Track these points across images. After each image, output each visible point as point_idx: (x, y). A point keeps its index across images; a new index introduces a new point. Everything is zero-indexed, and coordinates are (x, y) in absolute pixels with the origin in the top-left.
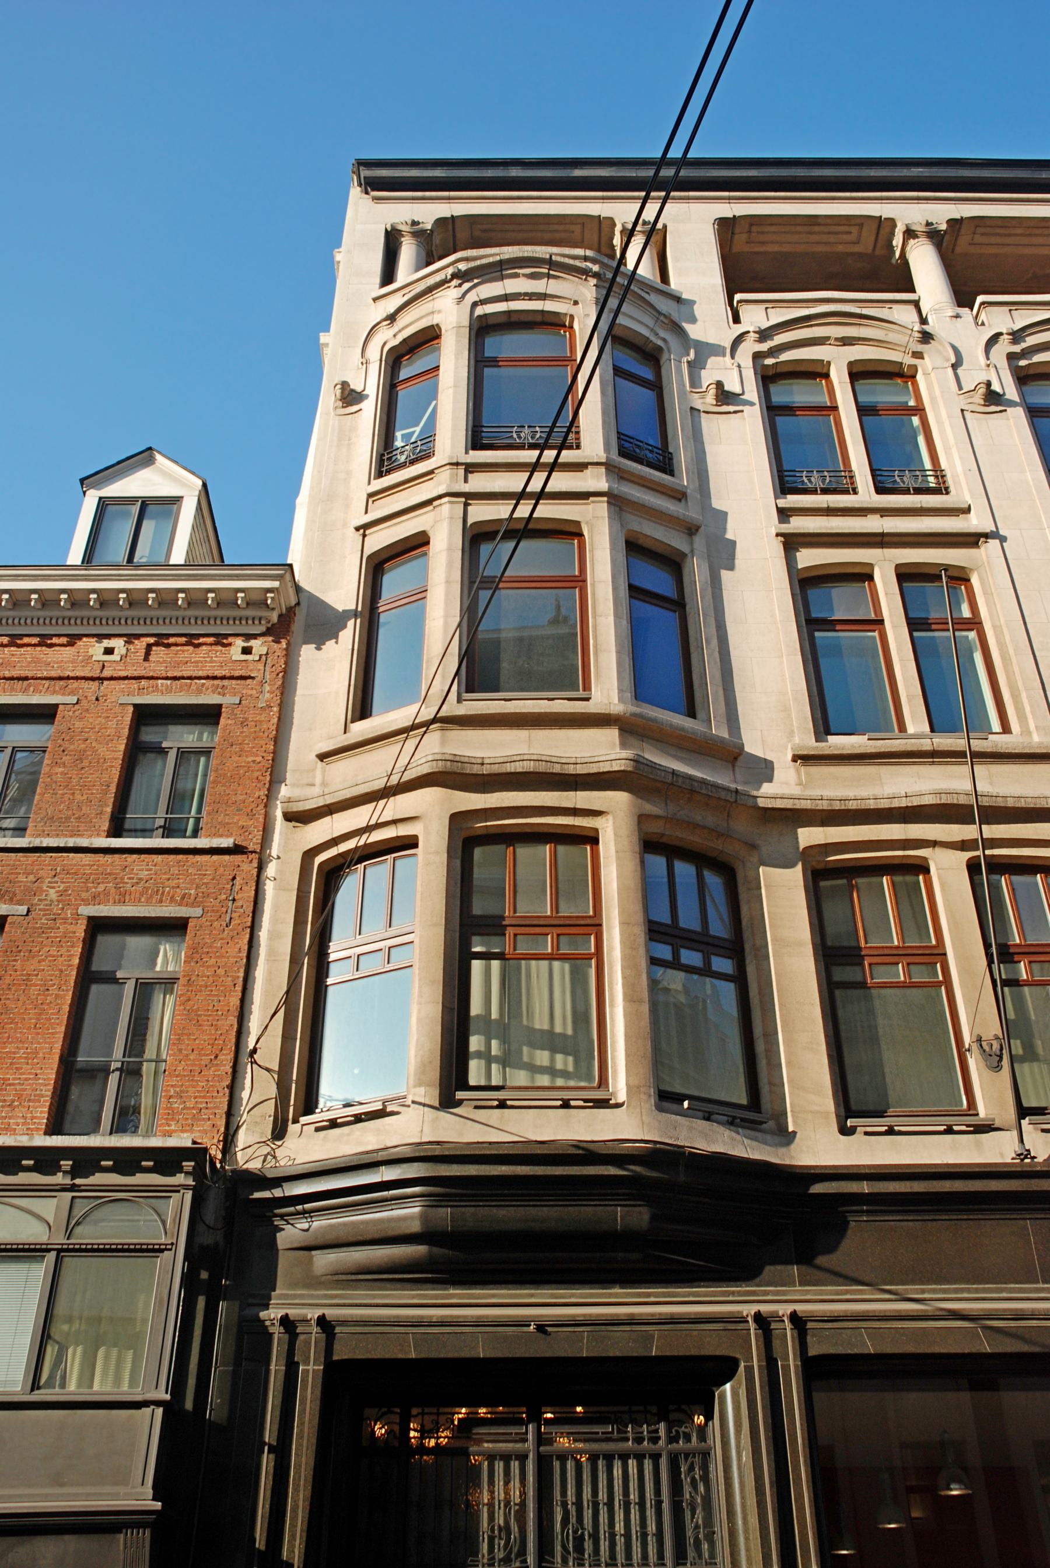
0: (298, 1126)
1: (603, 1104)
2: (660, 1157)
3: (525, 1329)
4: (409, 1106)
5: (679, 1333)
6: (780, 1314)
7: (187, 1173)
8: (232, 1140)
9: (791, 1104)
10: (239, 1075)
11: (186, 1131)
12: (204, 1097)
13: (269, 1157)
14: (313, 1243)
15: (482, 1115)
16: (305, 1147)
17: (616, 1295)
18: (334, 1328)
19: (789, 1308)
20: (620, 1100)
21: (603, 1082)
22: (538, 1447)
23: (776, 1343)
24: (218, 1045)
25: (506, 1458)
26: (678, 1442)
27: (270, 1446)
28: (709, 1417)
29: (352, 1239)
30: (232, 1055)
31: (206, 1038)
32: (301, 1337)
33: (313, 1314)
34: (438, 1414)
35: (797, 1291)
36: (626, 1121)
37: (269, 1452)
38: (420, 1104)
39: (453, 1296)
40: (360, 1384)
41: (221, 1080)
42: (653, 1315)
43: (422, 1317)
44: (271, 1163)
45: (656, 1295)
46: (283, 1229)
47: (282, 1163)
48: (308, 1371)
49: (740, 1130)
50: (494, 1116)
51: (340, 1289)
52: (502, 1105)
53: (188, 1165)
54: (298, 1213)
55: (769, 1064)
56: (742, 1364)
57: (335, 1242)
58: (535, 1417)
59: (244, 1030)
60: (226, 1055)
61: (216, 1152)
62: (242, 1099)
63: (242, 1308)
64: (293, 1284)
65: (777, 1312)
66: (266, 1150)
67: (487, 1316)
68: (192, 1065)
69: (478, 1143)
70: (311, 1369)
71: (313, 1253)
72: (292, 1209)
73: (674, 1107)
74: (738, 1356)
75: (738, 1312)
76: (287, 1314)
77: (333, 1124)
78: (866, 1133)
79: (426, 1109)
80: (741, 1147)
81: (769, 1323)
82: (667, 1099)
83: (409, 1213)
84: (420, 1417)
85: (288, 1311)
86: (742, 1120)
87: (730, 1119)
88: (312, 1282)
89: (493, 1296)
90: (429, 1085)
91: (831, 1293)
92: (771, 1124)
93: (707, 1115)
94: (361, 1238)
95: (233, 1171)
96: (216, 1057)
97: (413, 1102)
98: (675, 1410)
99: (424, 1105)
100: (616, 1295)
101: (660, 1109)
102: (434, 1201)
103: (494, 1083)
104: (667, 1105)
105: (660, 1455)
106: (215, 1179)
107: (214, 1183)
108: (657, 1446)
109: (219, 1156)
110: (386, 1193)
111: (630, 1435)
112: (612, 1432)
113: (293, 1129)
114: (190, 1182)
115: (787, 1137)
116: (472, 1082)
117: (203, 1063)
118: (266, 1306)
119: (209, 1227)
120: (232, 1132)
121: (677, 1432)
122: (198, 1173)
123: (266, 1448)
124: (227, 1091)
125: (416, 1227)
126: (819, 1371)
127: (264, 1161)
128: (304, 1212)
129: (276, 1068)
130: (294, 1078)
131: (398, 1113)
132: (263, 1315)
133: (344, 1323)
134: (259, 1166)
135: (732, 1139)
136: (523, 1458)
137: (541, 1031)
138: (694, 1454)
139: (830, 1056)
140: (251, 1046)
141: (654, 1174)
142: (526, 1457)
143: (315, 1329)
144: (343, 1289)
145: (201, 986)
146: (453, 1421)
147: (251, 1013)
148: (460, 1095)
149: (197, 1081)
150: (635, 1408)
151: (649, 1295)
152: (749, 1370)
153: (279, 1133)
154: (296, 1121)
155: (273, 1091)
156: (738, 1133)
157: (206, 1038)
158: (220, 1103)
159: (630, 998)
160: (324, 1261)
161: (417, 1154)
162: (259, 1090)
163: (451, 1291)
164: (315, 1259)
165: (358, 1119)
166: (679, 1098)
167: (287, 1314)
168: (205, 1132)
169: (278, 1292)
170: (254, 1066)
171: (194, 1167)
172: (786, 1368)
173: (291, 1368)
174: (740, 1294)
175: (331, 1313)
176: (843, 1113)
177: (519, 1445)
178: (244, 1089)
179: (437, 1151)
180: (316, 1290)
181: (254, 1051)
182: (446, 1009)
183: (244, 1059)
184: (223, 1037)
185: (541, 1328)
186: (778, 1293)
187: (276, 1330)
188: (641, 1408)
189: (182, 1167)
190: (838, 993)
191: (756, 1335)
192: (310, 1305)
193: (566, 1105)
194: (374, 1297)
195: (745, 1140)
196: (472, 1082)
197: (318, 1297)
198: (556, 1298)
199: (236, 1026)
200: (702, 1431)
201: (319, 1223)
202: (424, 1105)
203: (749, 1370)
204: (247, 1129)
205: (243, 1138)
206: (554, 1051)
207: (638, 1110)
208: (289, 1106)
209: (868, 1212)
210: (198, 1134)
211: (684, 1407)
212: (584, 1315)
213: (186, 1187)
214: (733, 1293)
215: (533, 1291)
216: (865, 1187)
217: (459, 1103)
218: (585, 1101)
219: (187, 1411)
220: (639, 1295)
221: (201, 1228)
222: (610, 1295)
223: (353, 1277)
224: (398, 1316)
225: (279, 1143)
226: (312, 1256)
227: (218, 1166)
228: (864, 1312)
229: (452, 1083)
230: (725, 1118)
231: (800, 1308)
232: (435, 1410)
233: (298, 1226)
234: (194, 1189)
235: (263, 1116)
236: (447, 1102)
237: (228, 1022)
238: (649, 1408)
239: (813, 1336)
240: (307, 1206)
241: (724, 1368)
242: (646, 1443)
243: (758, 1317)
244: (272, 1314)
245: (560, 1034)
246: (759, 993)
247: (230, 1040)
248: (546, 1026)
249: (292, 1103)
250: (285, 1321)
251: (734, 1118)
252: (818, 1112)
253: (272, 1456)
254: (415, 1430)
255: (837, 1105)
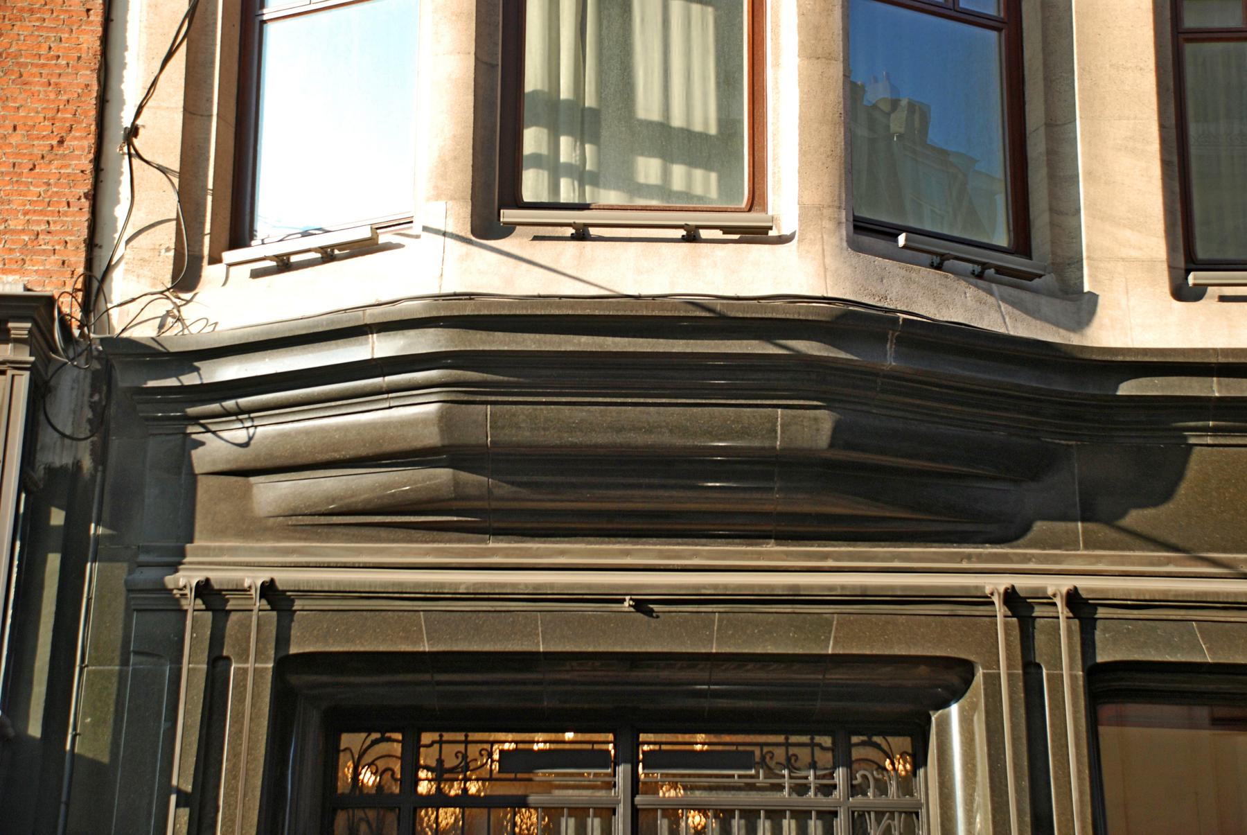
0: (220, 268)
1: (757, 235)
2: (845, 322)
3: (615, 607)
4: (418, 237)
5: (873, 618)
6: (1050, 592)
7: (18, 341)
8: (100, 289)
9: (1088, 246)
10: (108, 177)
11: (11, 272)
12: (41, 213)
13: (170, 320)
14: (253, 465)
15: (545, 252)
16: (231, 302)
17: (769, 555)
18: (291, 601)
19: (1065, 584)
20: (786, 231)
21: (757, 199)
22: (633, 797)
23: (1040, 639)
24: (64, 120)
25: (580, 813)
26: (865, 794)
27: (179, 792)
28: (919, 759)
29: (321, 457)
30: (91, 140)
31: (39, 106)
32: (234, 617)
33: (254, 579)
34: (466, 742)
35: (1080, 558)
36: (799, 265)
37: (178, 805)
38: (437, 232)
39: (494, 552)
40: (330, 694)
41: (73, 183)
42: (831, 588)
43: (442, 585)
44: (174, 330)
45: (838, 557)
46: (202, 444)
47: (194, 329)
48: (245, 671)
49: (994, 286)
50: (567, 254)
51: (300, 539)
52: (581, 235)
53: (20, 328)
54: (227, 413)
55: (1052, 176)
56: (980, 673)
57: (291, 462)
58: (628, 753)
59: (112, 95)
60: (81, 138)
61: (70, 307)
62: (115, 219)
63: (130, 572)
64: (219, 532)
65: (1044, 589)
66: (163, 306)
67: (552, 585)
68: (17, 155)
69: (540, 296)
70: (252, 672)
71: (253, 479)
72: (215, 407)
73: (881, 244)
74: (972, 658)
75: (977, 588)
76: (208, 580)
77: (284, 264)
78: (1223, 299)
79: (450, 242)
80: (997, 316)
81: (1031, 607)
82: (867, 232)
83: (415, 414)
84: (436, 746)
85: (211, 575)
86: (1000, 270)
87: (978, 269)
88: (250, 526)
89: (562, 553)
90: (452, 198)
91: (1141, 561)
92: (1049, 280)
93: (937, 260)
94: (337, 456)
95: (103, 341)
96: (61, 142)
97: (425, 229)
98: (863, 744)
99: (445, 234)
100: (769, 555)
101: (855, 246)
102: (461, 395)
103: (563, 198)
104: (867, 240)
105: (835, 814)
106: (71, 354)
107: (72, 360)
108: (829, 799)
109: (78, 314)
110: (379, 380)
111: (787, 782)
112: (756, 776)
113: (210, 273)
114: (25, 356)
115: (1082, 307)
116: (527, 197)
117: (36, 151)
118: (174, 567)
119: (63, 435)
120: (98, 273)
121: (864, 777)
122: (40, 341)
123: (173, 798)
124: (86, 203)
125: (432, 437)
126: (1108, 686)
127: (161, 326)
128: (240, 411)
129: (176, 166)
130: (210, 186)
131: (399, 246)
132: (170, 580)
133: (307, 593)
134: (154, 334)
135: (980, 301)
136: (607, 812)
137: (650, 124)
138: (892, 813)
139: (1165, 164)
140: (127, 122)
141: (842, 355)
142: (614, 811)
143: (258, 604)
144: (306, 540)
145: (22, 10)
146: (490, 755)
147: (123, 66)
148: (508, 215)
149: (27, 184)
150: (794, 739)
151: (825, 556)
152: (992, 682)
153: (185, 277)
154: (215, 259)
155: (169, 205)
156: (991, 293)
157: (39, 106)
158: (74, 224)
159: (810, 52)
160: (271, 493)
161: (434, 314)
162: (146, 205)
163: (491, 545)
164: (255, 490)
165: (328, 255)
166: (890, 233)
167: (208, 580)
168: (49, 274)
169: (197, 543)
170: (136, 161)
171: (30, 331)
172: (1056, 681)
173: (217, 663)
174: (980, 558)
175: (284, 578)
176: (1181, 263)
177: (601, 794)
178: (118, 202)
179: (469, 309)
180: (258, 540)
181: (133, 131)
182: (482, 65)
183: (115, 146)
184: (71, 107)
185: (641, 606)
186: (1046, 559)
187: (191, 604)
188: (805, 739)
189: (8, 330)
190: (1189, 49)
191: (1006, 625)
192: (248, 564)
193: (692, 236)
194: (359, 552)
195: (1003, 306)
196: (527, 197)
197: (262, 552)
198: (669, 558)
199: (95, 87)
200: (906, 785)
201: (267, 430)
202: (445, 234)
203: (992, 682)
204: (127, 270)
205: (120, 285)
206: (668, 157)
207: (818, 247)
208: (203, 235)
209: (1215, 430)
210: (34, 277)
211: (877, 739)
212: (716, 586)
213: (18, 365)
214: (969, 557)
215: (629, 547)
216: (1215, 388)
217: (507, 230)
218: (726, 230)
219: (33, 739)
220: (809, 556)
221: (47, 436)
222: (760, 555)
223: (323, 520)
224: (400, 584)
225: (187, 296)
226: (250, 486)
227: (76, 332)
228: (1197, 594)
229: (494, 198)
230: (970, 266)
231: (1083, 583)
232: (460, 736)
233: (224, 435)
234: (32, 368)
235: (156, 250)
236: (486, 226)
237: (80, 80)
238: (818, 739)
239: (1105, 630)
240: (243, 401)
241: (952, 678)
242: (811, 793)
243: (1011, 597)
244: (185, 579)
245: (682, 130)
246: (1044, 49)
247: (85, 113)
248: (655, 116)
249: (208, 229)
250: (204, 589)
251: (985, 266)
252: (1136, 260)
253: (185, 813)
254: (428, 768)
255: (1171, 248)
